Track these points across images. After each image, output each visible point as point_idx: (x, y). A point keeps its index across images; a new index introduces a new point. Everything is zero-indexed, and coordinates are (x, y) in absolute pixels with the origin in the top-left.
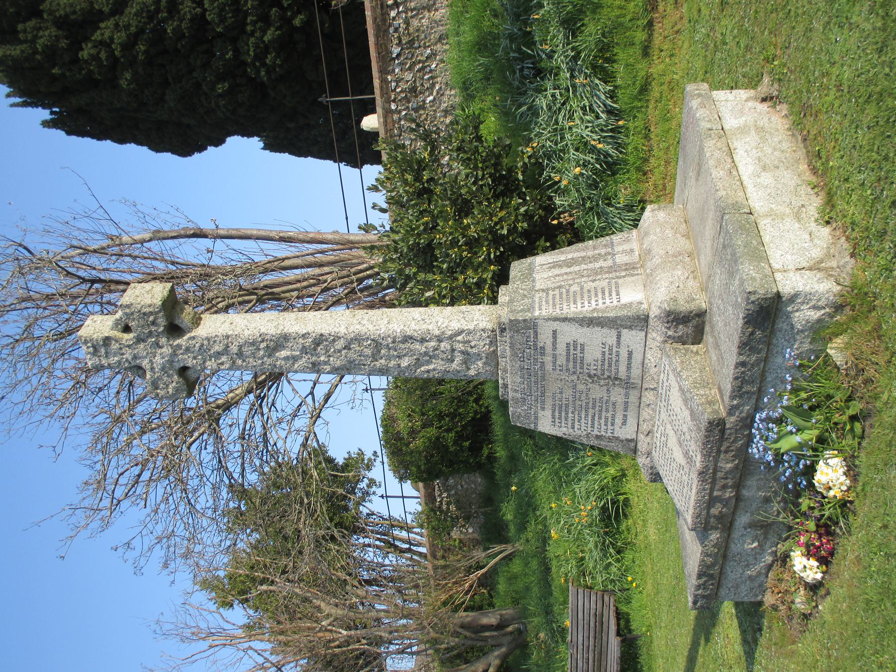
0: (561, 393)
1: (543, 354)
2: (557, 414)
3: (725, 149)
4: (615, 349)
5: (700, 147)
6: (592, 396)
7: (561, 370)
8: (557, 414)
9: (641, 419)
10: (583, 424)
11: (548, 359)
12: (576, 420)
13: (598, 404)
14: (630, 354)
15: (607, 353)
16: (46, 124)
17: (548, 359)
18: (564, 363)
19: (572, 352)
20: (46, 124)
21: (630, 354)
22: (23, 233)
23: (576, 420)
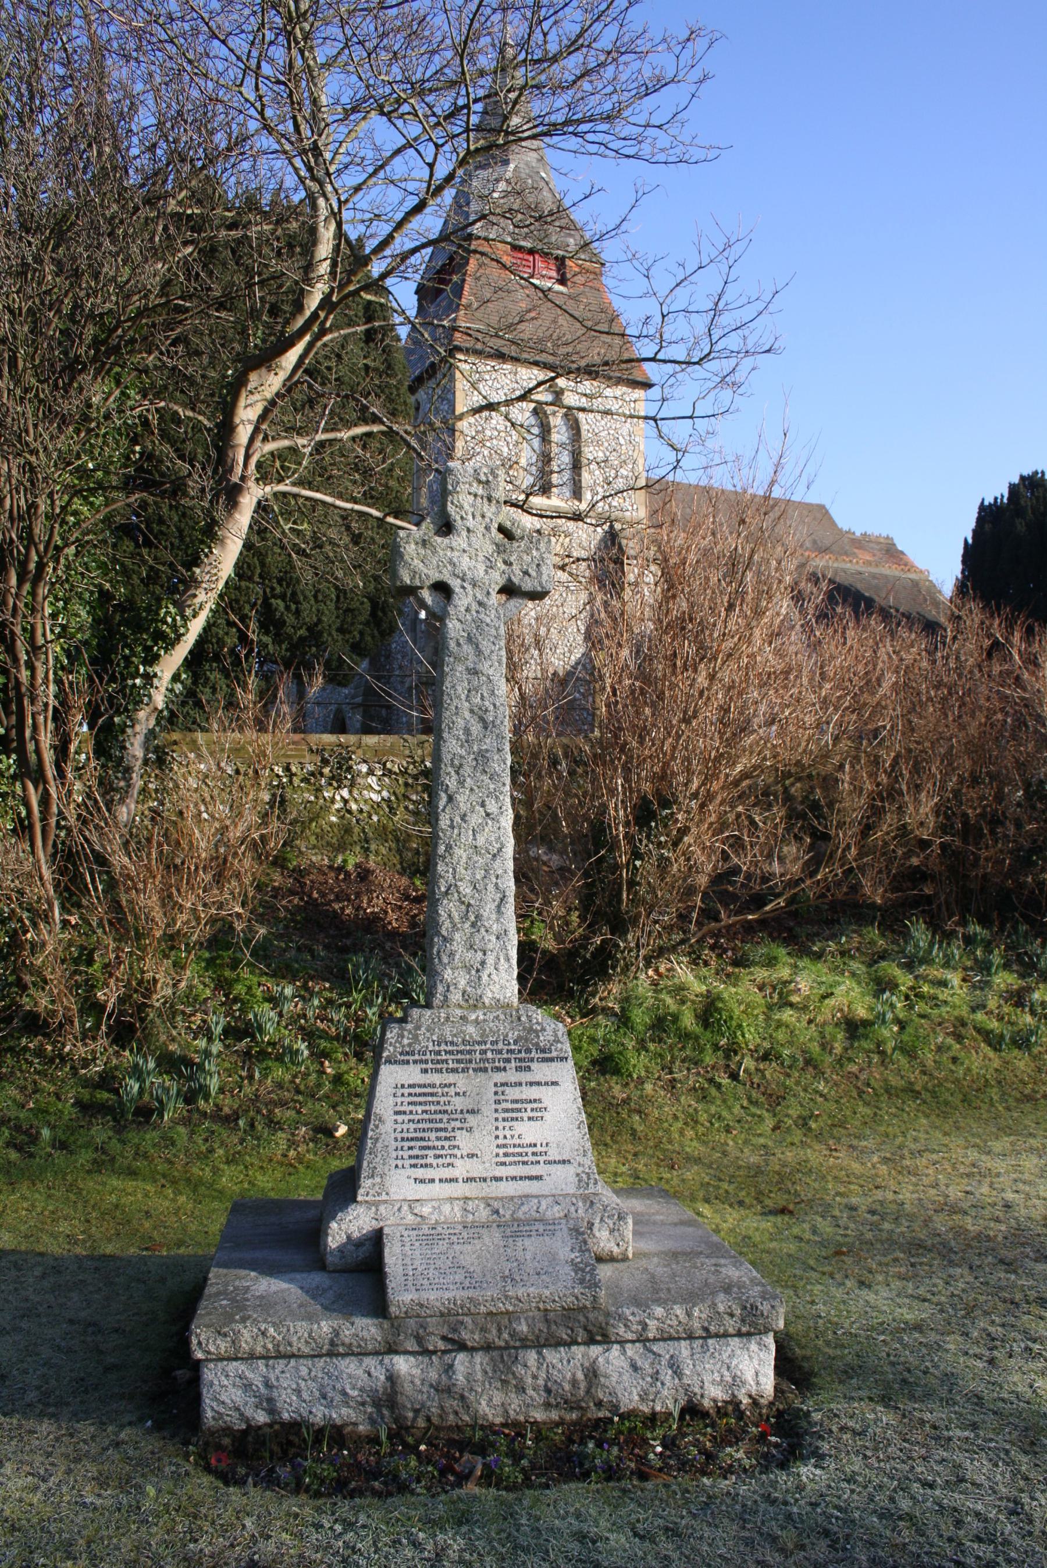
0: (457, 1094)
1: (518, 1069)
2: (418, 1090)
3: (775, 460)
4: (541, 1159)
5: (812, 874)
6: (458, 1133)
7: (496, 1093)
8: (418, 1090)
9: (487, 261)
10: (405, 1126)
11: (512, 1076)
12: (411, 1117)
13: (446, 1144)
14: (538, 1178)
15: (534, 1150)
16: (966, 540)
17: (512, 1076)
18: (509, 1098)
19: (529, 1106)
20: (966, 540)
21: (538, 1178)
22: (700, 1333)
23: (411, 1117)
